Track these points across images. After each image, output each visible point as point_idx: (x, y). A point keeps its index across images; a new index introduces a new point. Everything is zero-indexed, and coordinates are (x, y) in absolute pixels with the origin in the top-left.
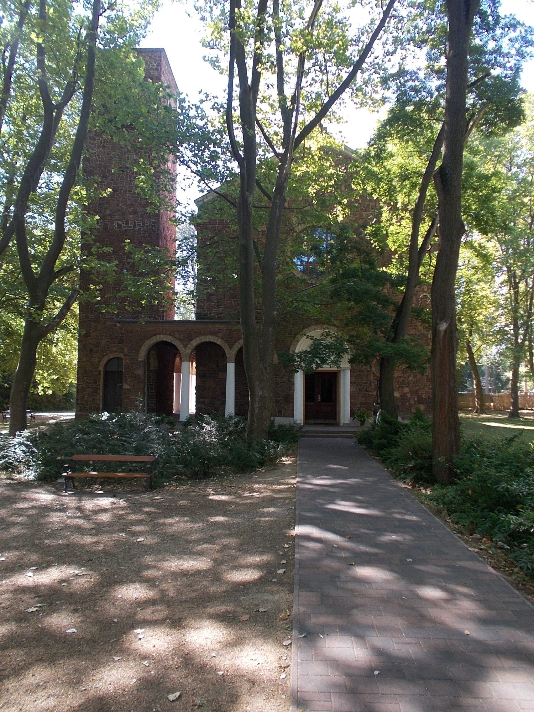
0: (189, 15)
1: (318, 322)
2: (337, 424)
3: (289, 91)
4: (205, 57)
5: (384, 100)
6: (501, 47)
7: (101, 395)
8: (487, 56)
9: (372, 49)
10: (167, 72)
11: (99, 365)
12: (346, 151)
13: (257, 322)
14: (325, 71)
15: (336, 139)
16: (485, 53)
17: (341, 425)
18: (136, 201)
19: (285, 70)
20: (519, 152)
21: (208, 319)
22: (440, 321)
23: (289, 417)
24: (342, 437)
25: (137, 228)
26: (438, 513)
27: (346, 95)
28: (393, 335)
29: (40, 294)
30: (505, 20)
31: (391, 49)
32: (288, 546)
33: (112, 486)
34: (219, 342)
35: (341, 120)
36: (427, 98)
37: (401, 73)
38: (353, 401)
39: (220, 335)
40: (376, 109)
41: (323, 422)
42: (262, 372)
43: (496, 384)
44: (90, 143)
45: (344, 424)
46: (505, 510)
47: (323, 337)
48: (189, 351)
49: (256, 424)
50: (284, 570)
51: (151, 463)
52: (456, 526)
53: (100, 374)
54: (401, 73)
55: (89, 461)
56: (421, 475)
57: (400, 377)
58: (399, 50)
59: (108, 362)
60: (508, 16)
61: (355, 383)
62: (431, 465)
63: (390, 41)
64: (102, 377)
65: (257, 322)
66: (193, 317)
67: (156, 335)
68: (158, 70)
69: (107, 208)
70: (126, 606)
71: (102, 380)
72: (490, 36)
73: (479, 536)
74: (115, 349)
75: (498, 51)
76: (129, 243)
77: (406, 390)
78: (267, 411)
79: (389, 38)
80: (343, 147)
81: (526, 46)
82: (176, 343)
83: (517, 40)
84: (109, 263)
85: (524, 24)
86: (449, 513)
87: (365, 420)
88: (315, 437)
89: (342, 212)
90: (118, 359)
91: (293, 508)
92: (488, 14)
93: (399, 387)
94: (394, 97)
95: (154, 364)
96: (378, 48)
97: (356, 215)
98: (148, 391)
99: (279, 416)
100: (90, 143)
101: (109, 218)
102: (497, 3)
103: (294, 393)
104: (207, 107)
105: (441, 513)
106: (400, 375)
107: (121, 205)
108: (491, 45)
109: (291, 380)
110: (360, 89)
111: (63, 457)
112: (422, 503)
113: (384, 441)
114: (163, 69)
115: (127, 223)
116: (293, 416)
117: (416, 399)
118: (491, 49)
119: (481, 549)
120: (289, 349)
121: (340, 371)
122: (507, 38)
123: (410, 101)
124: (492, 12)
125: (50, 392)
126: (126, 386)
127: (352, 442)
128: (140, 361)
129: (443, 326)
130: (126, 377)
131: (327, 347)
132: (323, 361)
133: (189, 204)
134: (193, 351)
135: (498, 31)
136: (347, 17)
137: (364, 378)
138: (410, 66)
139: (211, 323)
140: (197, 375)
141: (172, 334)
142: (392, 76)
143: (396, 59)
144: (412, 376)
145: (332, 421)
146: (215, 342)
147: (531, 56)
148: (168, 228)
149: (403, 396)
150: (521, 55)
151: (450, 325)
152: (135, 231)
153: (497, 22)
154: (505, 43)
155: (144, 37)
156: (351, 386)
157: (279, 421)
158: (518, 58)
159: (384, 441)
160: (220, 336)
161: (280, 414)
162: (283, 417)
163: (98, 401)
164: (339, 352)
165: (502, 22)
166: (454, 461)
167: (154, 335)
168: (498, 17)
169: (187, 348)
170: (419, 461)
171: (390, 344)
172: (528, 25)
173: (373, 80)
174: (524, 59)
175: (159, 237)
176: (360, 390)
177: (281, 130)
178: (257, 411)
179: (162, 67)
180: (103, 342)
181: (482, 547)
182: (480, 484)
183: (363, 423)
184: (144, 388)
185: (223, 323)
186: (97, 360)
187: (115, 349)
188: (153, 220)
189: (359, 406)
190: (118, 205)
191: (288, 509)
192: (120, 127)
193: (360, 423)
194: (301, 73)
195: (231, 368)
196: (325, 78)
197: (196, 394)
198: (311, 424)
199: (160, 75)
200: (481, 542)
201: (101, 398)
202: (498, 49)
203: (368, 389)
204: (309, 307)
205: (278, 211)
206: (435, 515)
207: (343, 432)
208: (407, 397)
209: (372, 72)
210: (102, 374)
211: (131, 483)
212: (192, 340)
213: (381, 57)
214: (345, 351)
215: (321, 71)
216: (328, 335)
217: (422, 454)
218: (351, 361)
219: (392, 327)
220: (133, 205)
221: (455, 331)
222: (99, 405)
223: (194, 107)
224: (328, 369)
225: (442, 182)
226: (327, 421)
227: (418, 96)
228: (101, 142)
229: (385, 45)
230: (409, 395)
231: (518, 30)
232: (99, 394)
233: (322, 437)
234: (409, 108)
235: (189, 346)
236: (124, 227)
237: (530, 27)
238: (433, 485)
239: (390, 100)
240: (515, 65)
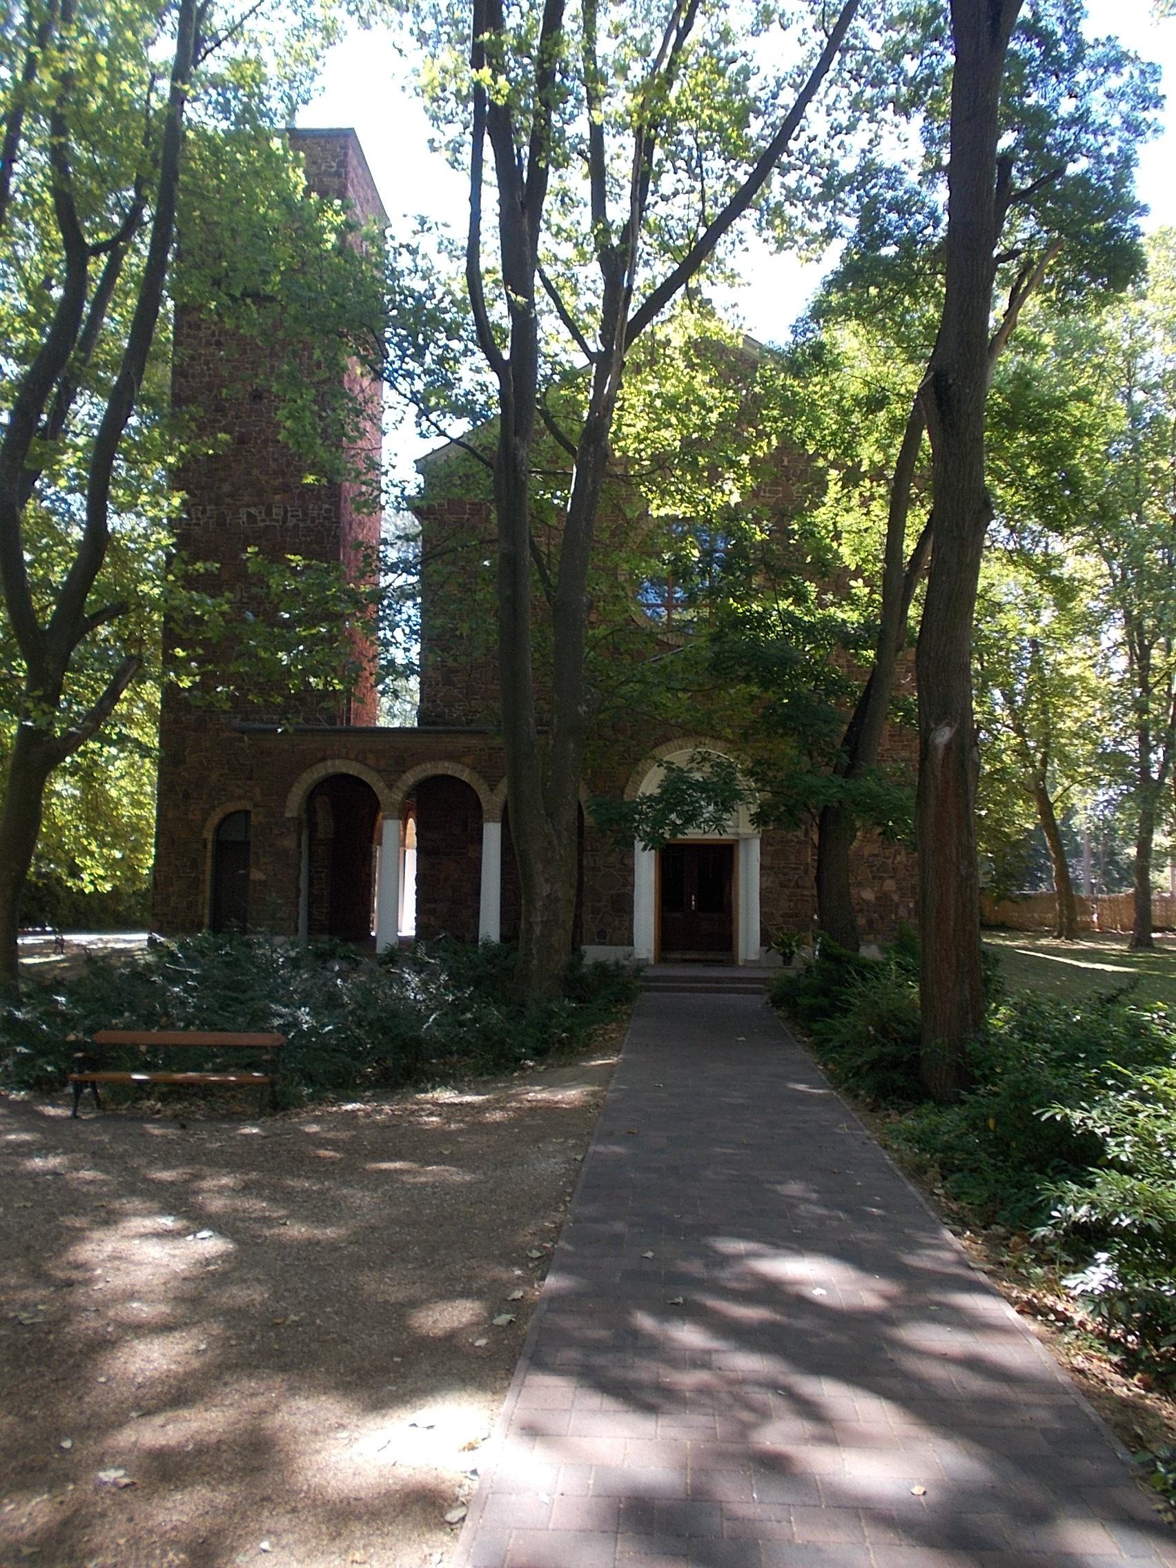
0: (400, 51)
1: (690, 732)
2: (732, 962)
3: (618, 212)
4: (433, 140)
5: (831, 233)
6: (1088, 110)
7: (208, 894)
8: (1058, 131)
9: (803, 122)
10: (362, 181)
12: (749, 349)
13: (539, 732)
14: (698, 171)
15: (725, 320)
16: (1054, 125)
17: (741, 963)
18: (288, 464)
19: (609, 170)
20: (1147, 359)
21: (445, 724)
22: (936, 724)
23: (622, 944)
24: (738, 991)
25: (291, 522)
26: (917, 1172)
27: (746, 223)
28: (846, 759)
29: (51, 666)
30: (1096, 50)
31: (843, 118)
32: (539, 1254)
33: (186, 1104)
34: (465, 776)
35: (737, 280)
36: (926, 228)
37: (869, 170)
38: (766, 909)
39: (468, 760)
40: (815, 257)
41: (702, 957)
42: (550, 842)
43: (1106, 873)
44: (188, 336)
45: (746, 961)
46: (1070, 1166)
47: (694, 765)
48: (398, 796)
49: (535, 962)
50: (509, 1317)
51: (278, 1049)
52: (954, 1207)
53: (205, 846)
54: (869, 170)
55: (138, 1045)
56: (894, 1080)
57: (876, 855)
58: (863, 124)
59: (223, 821)
60: (1103, 39)
61: (771, 868)
62: (917, 1056)
63: (845, 103)
64: (209, 854)
65: (539, 732)
66: (416, 724)
67: (323, 759)
68: (340, 176)
69: (223, 480)
70: (108, 1404)
71: (209, 861)
72: (1062, 86)
73: (1002, 1230)
74: (239, 792)
75: (1080, 120)
76: (256, 554)
77: (890, 885)
78: (562, 931)
79: (842, 96)
80: (740, 340)
81: (1145, 109)
82: (369, 777)
83: (1123, 94)
84: (212, 597)
85: (1137, 58)
86: (945, 1173)
87: (792, 953)
88: (719, 991)
89: (738, 484)
90: (247, 813)
91: (579, 1157)
92: (1059, 36)
93: (874, 877)
94: (850, 224)
95: (326, 825)
96: (816, 121)
97: (777, 492)
98: (311, 884)
99: (600, 944)
100: (188, 336)
101: (229, 500)
102: (1078, 9)
104: (427, 243)
105: (925, 1173)
106: (876, 852)
107: (256, 472)
108: (1067, 107)
109: (626, 862)
110: (777, 210)
111: (81, 1035)
112: (885, 1147)
113: (823, 1001)
114: (352, 175)
115: (269, 512)
116: (631, 943)
117: (911, 905)
118: (1066, 116)
119: (1001, 1264)
120: (623, 792)
121: (737, 841)
122: (1102, 90)
123: (889, 235)
124: (1067, 32)
125: (108, 887)
126: (257, 875)
127: (757, 1002)
128: (289, 819)
129: (943, 736)
131: (702, 787)
132: (690, 819)
133: (394, 467)
134: (408, 795)
135: (1082, 76)
136: (750, 52)
137: (793, 858)
138: (888, 155)
139: (448, 732)
140: (418, 849)
141: (361, 759)
142: (849, 179)
143: (858, 140)
144: (903, 852)
147: (1156, 131)
148: (361, 524)
149: (883, 899)
150: (1133, 128)
151: (958, 732)
152: (287, 530)
153: (1078, 56)
154: (1096, 103)
155: (305, 102)
157: (594, 953)
158: (1126, 135)
159: (823, 1001)
161: (602, 938)
162: (611, 944)
164: (726, 798)
165: (1091, 54)
166: (968, 1048)
168: (1080, 43)
169: (395, 790)
170: (890, 1048)
171: (840, 780)
172: (1145, 59)
173: (808, 190)
174: (1140, 138)
175: (338, 543)
176: (782, 885)
177: (599, 303)
178: (538, 930)
179: (350, 169)
181: (1006, 1258)
182: (1012, 1106)
183: (788, 959)
184: (297, 879)
185: (471, 733)
187: (239, 792)
188: (327, 506)
189: (781, 920)
190: (249, 474)
191: (568, 1162)
192: (238, 294)
193: (781, 958)
194: (643, 177)
195: (492, 834)
196: (698, 185)
197: (417, 893)
198: (676, 961)
199: (345, 187)
200: (1007, 1246)
201: (207, 901)
202: (1081, 116)
203: (800, 883)
204: (665, 698)
205: (589, 480)
206: (910, 1176)
207: (740, 980)
208: (892, 900)
209: (803, 173)
210: (210, 847)
211: (233, 1097)
212: (404, 772)
213: (822, 137)
214: (738, 795)
215: (689, 171)
216: (704, 759)
217: (898, 1032)
218: (759, 819)
219: (847, 740)
220: (283, 473)
221: (972, 747)
222: (202, 916)
223: (403, 250)
224: (700, 837)
225: (939, 406)
226: (710, 956)
227: (906, 224)
228: (213, 334)
229: (833, 112)
230: (896, 897)
231: (1126, 71)
232: (203, 892)
233: (692, 990)
234: (889, 251)
235: (399, 784)
236: (263, 521)
237: (1150, 64)
238: (920, 1103)
239: (844, 233)
240: (1120, 150)
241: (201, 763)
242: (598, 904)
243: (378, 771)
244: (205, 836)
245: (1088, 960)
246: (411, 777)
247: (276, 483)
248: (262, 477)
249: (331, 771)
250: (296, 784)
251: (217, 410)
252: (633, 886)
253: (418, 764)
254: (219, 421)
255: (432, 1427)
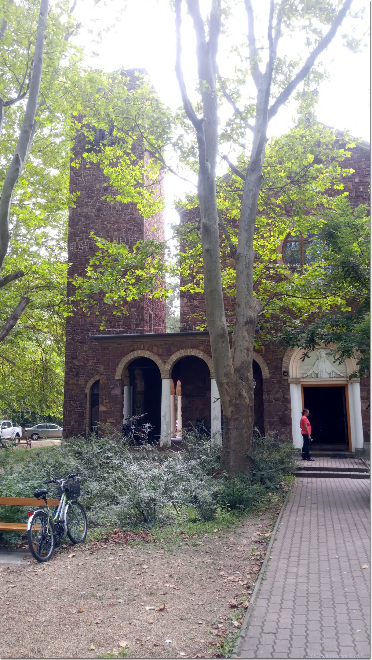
7: (88, 419)
11: (85, 387)
18: (120, 218)
39: (202, 348)
53: (86, 397)
67: (133, 350)
71: (88, 403)
103: (290, 413)
107: (105, 223)
109: (286, 397)
120: (282, 361)
130: (102, 398)
145: (343, 447)
146: (197, 355)
156: (362, 403)
160: (203, 349)
163: (84, 426)
167: (131, 351)
169: (167, 364)
180: (90, 363)
186: (83, 383)
188: (137, 236)
190: (103, 224)
210: (88, 397)
212: (171, 355)
220: (118, 223)
235: (169, 361)
241: (84, 358)
242: (272, 420)
243: (159, 355)
244: (86, 392)
245: (306, 471)
246: (174, 358)
247: (115, 227)
248: (108, 225)
249: (136, 356)
250: (120, 363)
251: (89, 198)
252: (291, 410)
253: (178, 350)
254: (90, 202)
255: (333, 60)
